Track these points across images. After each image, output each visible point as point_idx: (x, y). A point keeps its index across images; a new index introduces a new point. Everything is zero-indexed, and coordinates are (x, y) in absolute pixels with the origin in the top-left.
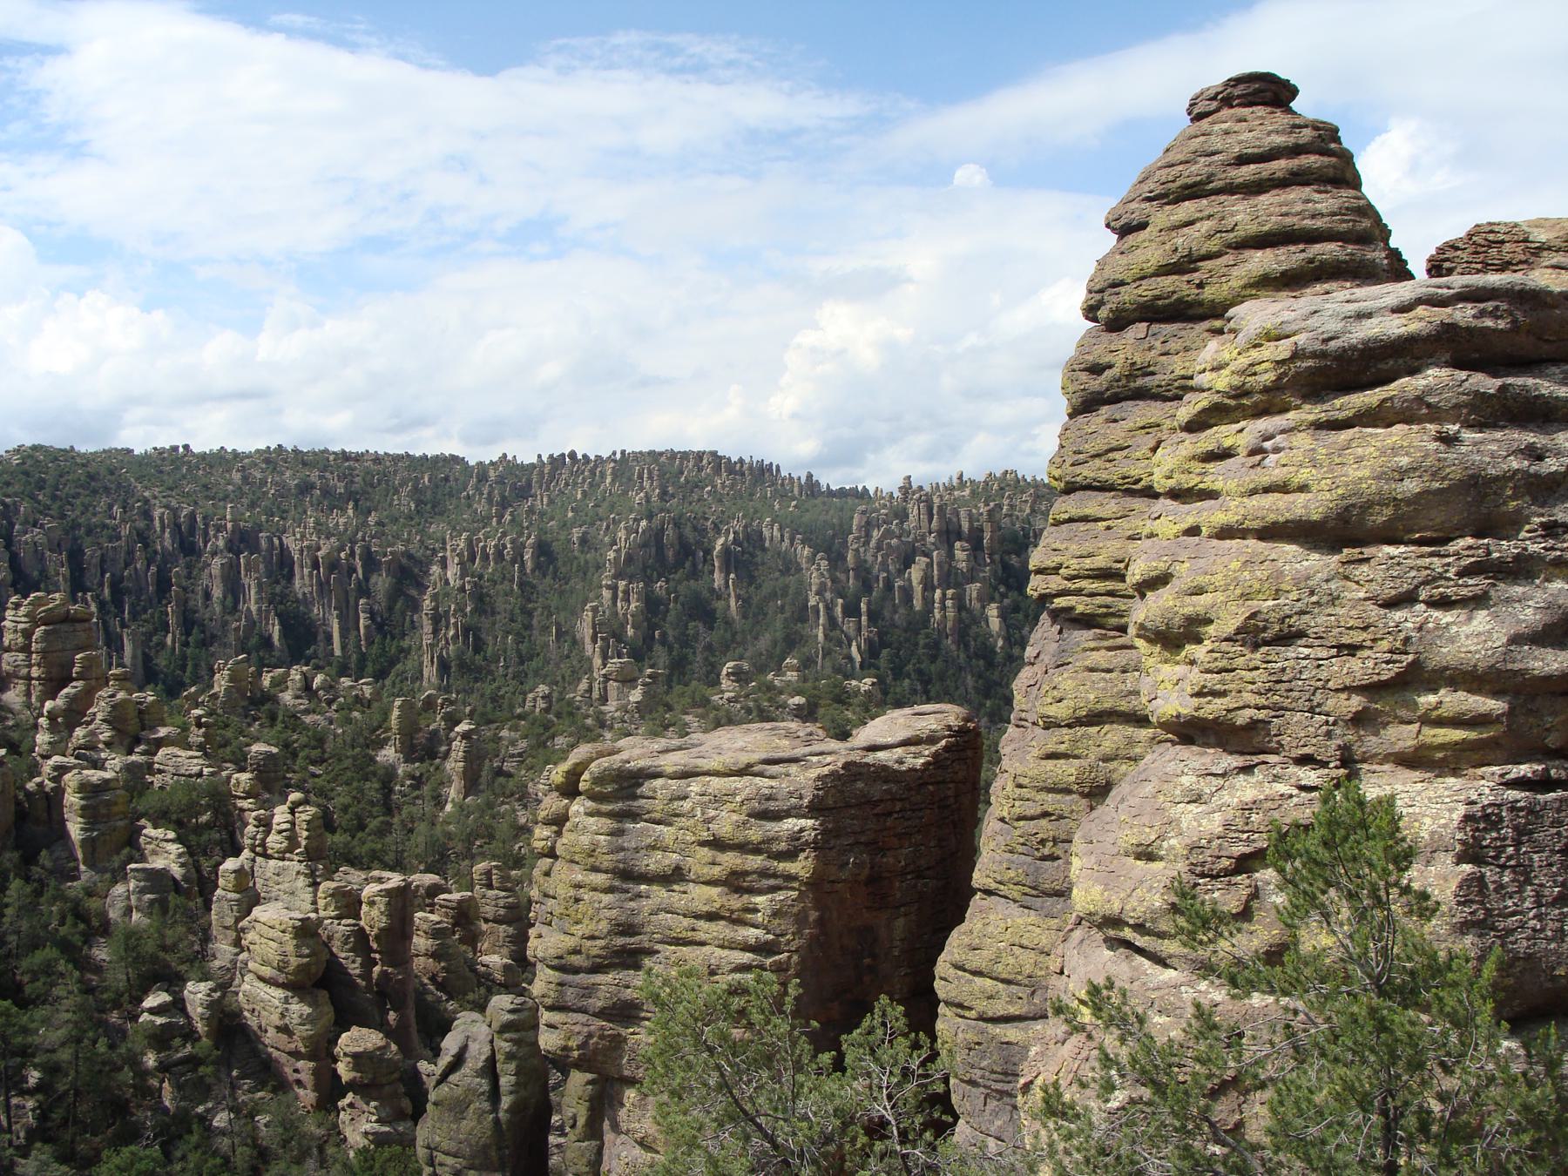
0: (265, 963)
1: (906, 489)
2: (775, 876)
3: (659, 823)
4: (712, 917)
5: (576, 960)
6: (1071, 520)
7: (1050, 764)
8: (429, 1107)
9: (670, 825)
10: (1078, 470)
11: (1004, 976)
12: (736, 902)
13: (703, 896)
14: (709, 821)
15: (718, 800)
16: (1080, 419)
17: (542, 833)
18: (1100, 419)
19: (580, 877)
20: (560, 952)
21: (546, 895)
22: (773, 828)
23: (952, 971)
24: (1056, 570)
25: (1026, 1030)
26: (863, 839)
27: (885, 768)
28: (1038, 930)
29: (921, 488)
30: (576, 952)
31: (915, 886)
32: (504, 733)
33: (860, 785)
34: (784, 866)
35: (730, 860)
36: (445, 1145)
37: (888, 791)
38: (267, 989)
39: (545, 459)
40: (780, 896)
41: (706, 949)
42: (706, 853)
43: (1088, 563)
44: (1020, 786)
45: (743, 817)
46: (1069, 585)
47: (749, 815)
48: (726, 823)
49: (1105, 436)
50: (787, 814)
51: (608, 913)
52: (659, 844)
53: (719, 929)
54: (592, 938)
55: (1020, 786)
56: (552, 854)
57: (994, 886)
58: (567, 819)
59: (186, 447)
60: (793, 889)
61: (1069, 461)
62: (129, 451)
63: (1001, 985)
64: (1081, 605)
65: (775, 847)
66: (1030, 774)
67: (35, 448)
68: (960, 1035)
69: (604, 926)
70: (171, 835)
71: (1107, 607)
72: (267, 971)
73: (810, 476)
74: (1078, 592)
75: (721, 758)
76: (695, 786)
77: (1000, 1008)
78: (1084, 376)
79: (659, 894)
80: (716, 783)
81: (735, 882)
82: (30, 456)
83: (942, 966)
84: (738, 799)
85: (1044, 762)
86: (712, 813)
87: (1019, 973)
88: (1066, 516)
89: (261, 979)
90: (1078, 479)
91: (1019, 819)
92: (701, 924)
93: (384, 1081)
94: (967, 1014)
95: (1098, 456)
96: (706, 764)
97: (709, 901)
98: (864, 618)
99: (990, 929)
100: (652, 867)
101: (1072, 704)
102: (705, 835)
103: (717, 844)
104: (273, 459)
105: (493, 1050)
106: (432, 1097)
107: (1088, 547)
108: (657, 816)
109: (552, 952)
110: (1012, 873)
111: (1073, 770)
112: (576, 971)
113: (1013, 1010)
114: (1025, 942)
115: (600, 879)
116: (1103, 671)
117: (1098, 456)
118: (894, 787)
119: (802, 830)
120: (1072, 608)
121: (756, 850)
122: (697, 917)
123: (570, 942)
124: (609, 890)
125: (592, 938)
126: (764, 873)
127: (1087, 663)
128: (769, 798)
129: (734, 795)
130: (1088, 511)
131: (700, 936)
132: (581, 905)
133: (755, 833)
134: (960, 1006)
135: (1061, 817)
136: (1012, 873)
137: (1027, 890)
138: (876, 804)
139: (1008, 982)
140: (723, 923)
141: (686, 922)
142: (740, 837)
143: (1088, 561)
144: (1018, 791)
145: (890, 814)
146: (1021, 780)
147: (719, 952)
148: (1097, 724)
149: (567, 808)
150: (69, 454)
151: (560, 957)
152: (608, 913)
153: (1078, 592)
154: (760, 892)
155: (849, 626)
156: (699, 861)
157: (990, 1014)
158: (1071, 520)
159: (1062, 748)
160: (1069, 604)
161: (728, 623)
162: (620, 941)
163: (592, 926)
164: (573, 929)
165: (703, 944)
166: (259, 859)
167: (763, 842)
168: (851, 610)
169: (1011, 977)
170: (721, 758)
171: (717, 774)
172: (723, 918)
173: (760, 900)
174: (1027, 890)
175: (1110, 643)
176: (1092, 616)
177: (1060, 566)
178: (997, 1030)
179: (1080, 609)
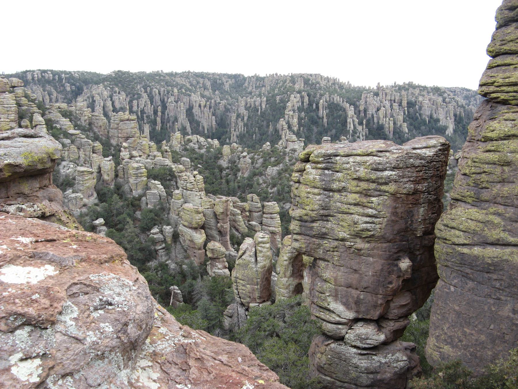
0: (186, 221)
1: (378, 88)
2: (380, 191)
3: (338, 172)
4: (355, 205)
5: (305, 218)
6: (498, 66)
7: (487, 154)
8: (236, 265)
9: (342, 172)
10: (502, 47)
11: (463, 229)
12: (364, 200)
13: (353, 197)
14: (357, 171)
15: (359, 164)
16: (499, 30)
17: (295, 175)
18: (513, 28)
19: (309, 190)
20: (301, 215)
21: (296, 196)
22: (380, 174)
23: (443, 227)
24: (492, 84)
25: (470, 249)
26: (412, 179)
27: (420, 155)
28: (478, 214)
29: (383, 86)
30: (306, 215)
31: (428, 197)
32: (256, 156)
33: (412, 160)
34: (383, 188)
35: (364, 185)
36: (240, 277)
37: (421, 163)
38: (186, 229)
39: (268, 75)
40: (381, 198)
41: (353, 216)
42: (355, 183)
43: (507, 80)
44: (475, 162)
45: (369, 170)
46: (498, 89)
47: (372, 170)
48: (362, 172)
49: (515, 33)
50: (385, 170)
51: (318, 202)
52: (339, 180)
53: (359, 209)
54: (313, 210)
55: (475, 162)
56: (299, 182)
57: (460, 198)
58: (305, 170)
59: (162, 71)
60: (386, 196)
61: (498, 44)
62: (145, 72)
63: (462, 233)
64: (503, 96)
65: (380, 181)
66: (480, 157)
67: (118, 71)
68: (444, 250)
69: (316, 207)
70: (160, 183)
71: (514, 96)
72: (186, 224)
73: (348, 82)
74: (502, 92)
75: (361, 150)
76: (351, 159)
77: (462, 241)
78: (506, 12)
79: (337, 196)
80: (358, 158)
81: (366, 194)
82: (117, 74)
83: (439, 225)
84: (368, 164)
85: (485, 154)
86: (358, 169)
87: (469, 229)
88: (496, 64)
89: (184, 226)
90: (502, 51)
91: (473, 173)
92: (352, 207)
93: (220, 257)
94: (447, 242)
95: (512, 41)
96: (355, 152)
97: (355, 199)
98: (364, 126)
99: (459, 213)
100: (335, 187)
101: (498, 132)
102: (355, 176)
103: (359, 179)
104: (186, 75)
105: (256, 250)
106: (237, 262)
107: (507, 74)
108: (337, 169)
109: (298, 215)
110: (469, 193)
111: (497, 156)
112: (306, 221)
113: (466, 242)
114: (473, 218)
115: (316, 191)
116: (511, 120)
117: (512, 41)
118: (423, 161)
119: (391, 175)
120: (498, 97)
121: (373, 182)
122: (350, 204)
123: (304, 212)
124: (319, 194)
125: (313, 210)
126: (376, 190)
127: (504, 117)
128: (379, 164)
129: (366, 162)
130: (506, 62)
131: (352, 211)
132: (308, 199)
133: (373, 176)
134: (446, 239)
135: (490, 173)
136: (469, 193)
137: (474, 199)
138: (417, 167)
139: (465, 232)
140: (359, 207)
141: (346, 206)
142: (368, 177)
143: (507, 80)
144: (473, 164)
145: (421, 171)
146: (475, 160)
147: (357, 217)
148: (508, 139)
149: (305, 166)
150: (128, 73)
151: (300, 217)
152: (318, 202)
153: (502, 92)
154: (374, 197)
155: (360, 128)
156: (352, 185)
157: (457, 243)
158: (498, 66)
159: (493, 148)
160: (498, 96)
161: (323, 125)
162: (322, 212)
163: (312, 206)
164: (306, 207)
165: (352, 214)
166: (184, 191)
167: (376, 179)
168: (361, 123)
169: (465, 230)
170: (361, 150)
171: (359, 155)
172: (360, 205)
173: (374, 199)
174: (474, 199)
175: (512, 111)
176: (507, 100)
177: (494, 82)
178: (459, 249)
179: (502, 97)
